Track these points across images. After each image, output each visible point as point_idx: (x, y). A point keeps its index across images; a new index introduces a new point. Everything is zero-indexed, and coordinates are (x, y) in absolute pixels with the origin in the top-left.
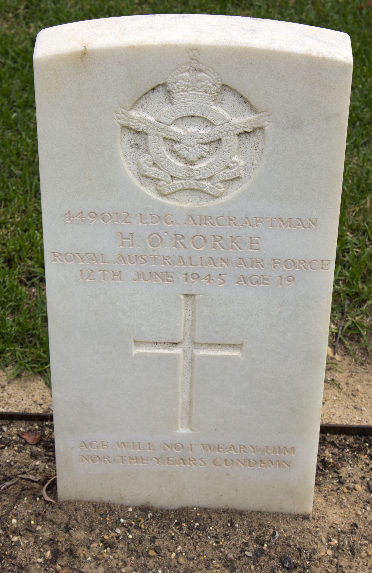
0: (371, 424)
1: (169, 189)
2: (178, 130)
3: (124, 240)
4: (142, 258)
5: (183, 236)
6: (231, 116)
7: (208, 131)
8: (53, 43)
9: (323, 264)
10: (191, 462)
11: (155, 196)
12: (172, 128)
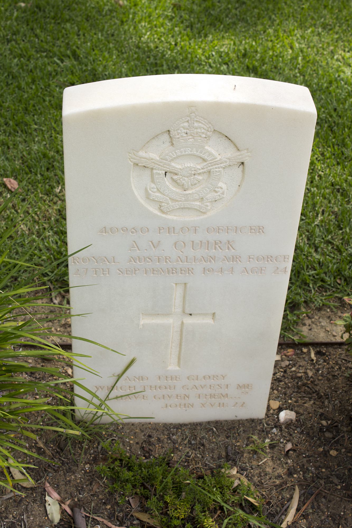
2: (176, 165)
3: (188, 321)
6: (217, 150)
8: (80, 100)
12: (173, 164)
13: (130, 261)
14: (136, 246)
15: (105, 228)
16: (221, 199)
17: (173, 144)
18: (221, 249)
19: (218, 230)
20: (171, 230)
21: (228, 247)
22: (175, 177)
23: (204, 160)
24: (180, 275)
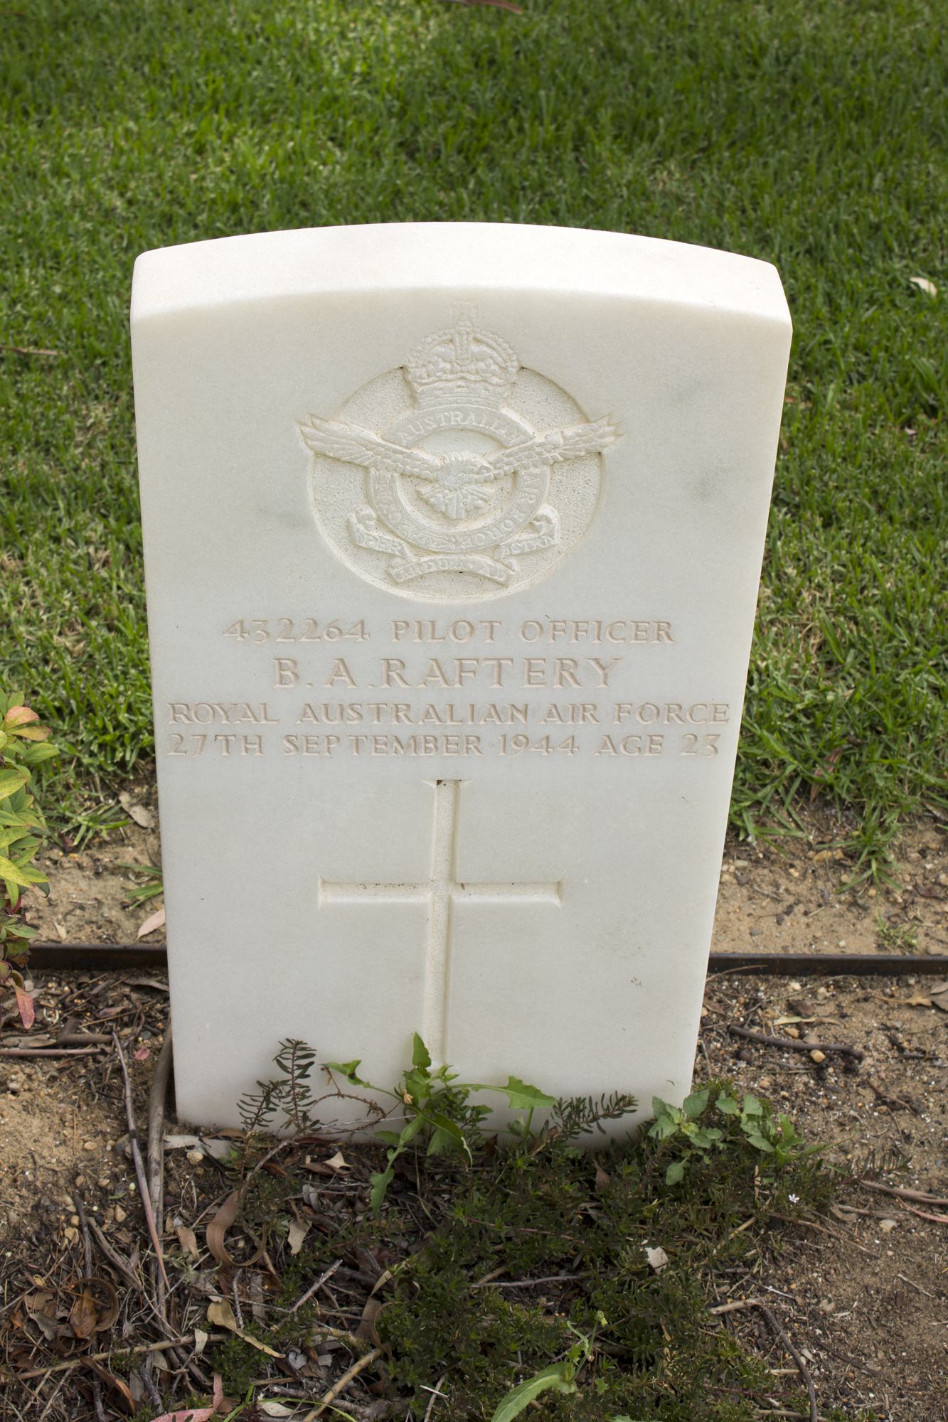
2: (428, 456)
3: (461, 899)
6: (534, 423)
8: (174, 283)
9: (718, 711)
13: (305, 714)
14: (438, 673)
15: (242, 622)
16: (545, 549)
17: (414, 398)
18: (576, 681)
19: (555, 628)
20: (426, 628)
21: (561, 676)
22: (425, 490)
23: (502, 445)
24: (647, 754)
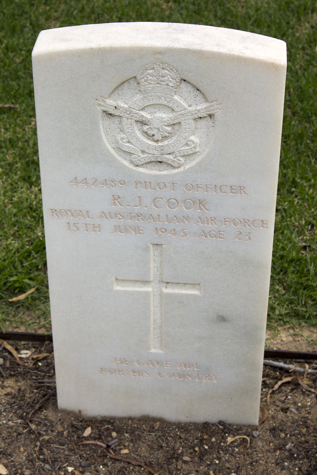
0: (316, 350)
1: (140, 161)
4: (120, 215)
5: (119, 197)
7: (171, 115)
8: (51, 42)
10: (207, 378)
11: (131, 167)
